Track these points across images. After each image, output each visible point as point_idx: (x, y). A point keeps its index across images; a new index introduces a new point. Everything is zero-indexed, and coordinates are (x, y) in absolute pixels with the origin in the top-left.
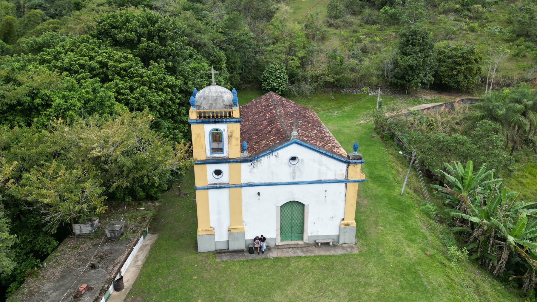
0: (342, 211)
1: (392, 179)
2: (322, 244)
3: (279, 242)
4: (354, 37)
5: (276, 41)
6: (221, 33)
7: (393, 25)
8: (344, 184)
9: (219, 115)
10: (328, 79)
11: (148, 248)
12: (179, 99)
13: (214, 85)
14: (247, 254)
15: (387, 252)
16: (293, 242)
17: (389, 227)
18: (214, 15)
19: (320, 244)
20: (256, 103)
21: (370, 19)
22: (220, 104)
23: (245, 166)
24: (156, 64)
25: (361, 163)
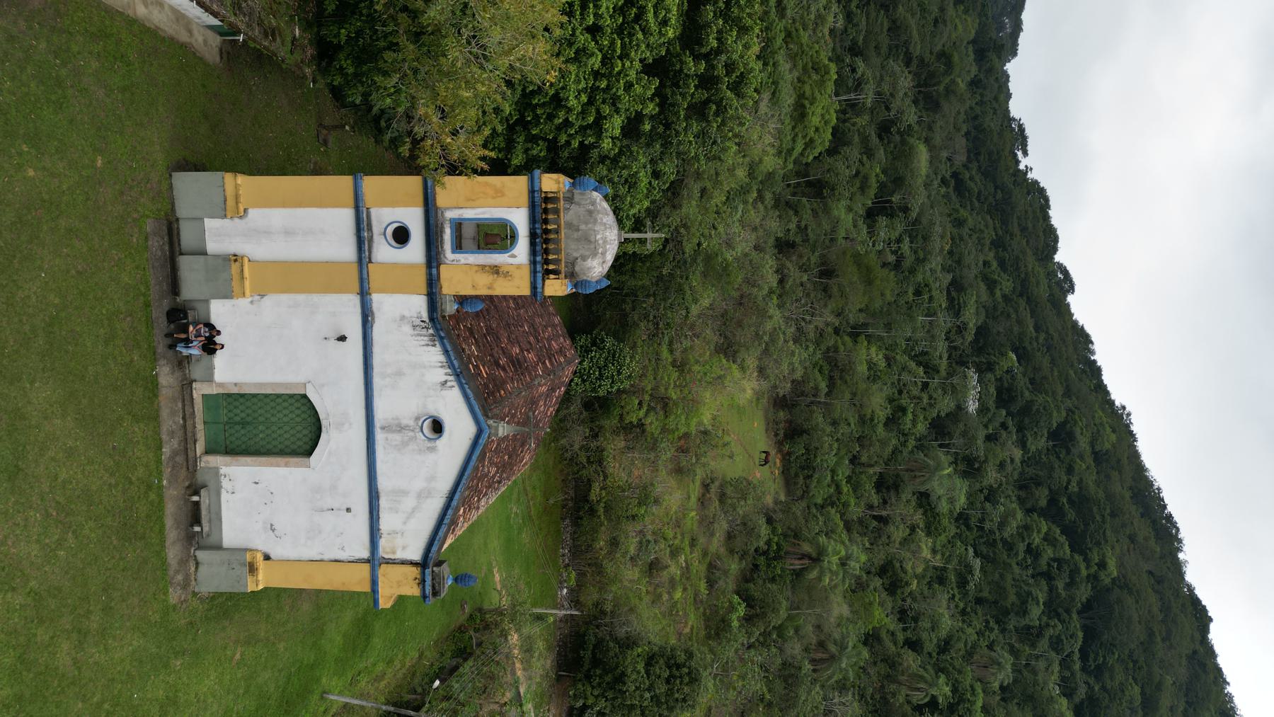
0: (292, 553)
1: (362, 666)
2: (197, 504)
3: (200, 390)
4: (682, 541)
5: (681, 366)
6: (699, 244)
7: (707, 627)
8: (365, 554)
9: (551, 246)
10: (596, 488)
11: (183, 37)
12: (568, 143)
13: (620, 236)
14: (166, 304)
15: (171, 679)
16: (200, 426)
17: (239, 676)
18: (736, 228)
19: (195, 498)
20: (554, 326)
21: (718, 574)
22: (576, 250)
23: (418, 304)
24: (649, 93)
25: (424, 597)
